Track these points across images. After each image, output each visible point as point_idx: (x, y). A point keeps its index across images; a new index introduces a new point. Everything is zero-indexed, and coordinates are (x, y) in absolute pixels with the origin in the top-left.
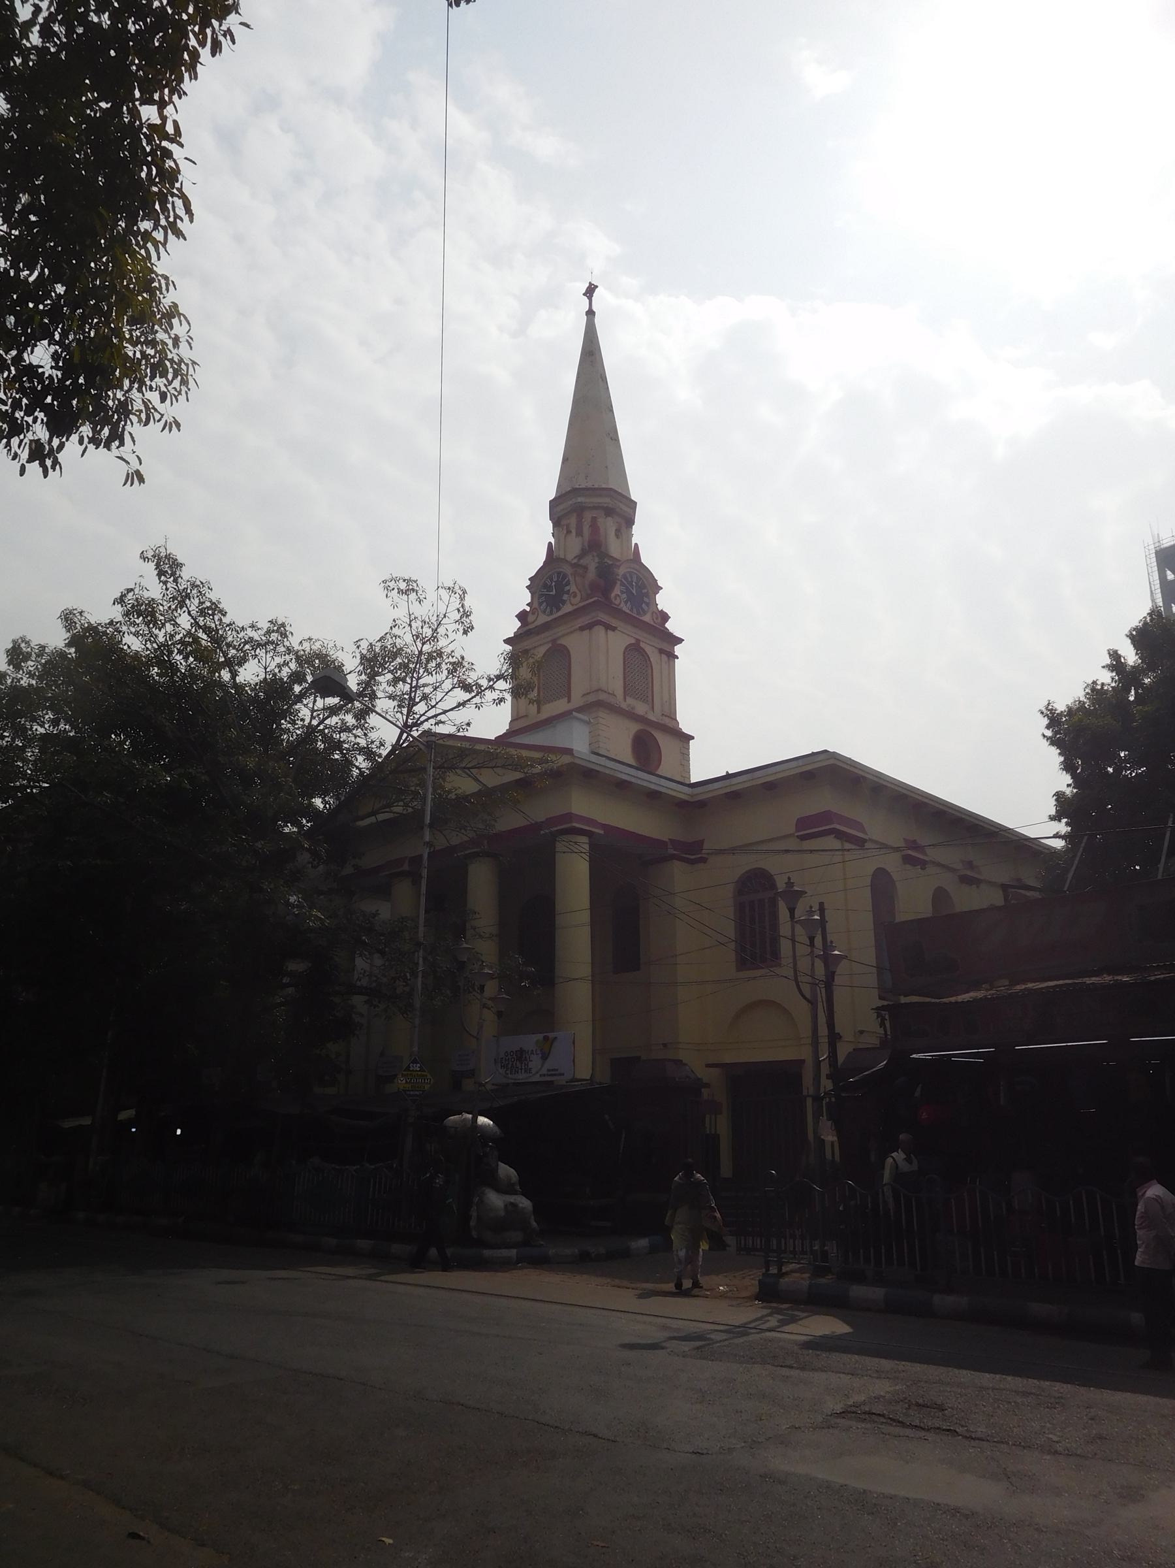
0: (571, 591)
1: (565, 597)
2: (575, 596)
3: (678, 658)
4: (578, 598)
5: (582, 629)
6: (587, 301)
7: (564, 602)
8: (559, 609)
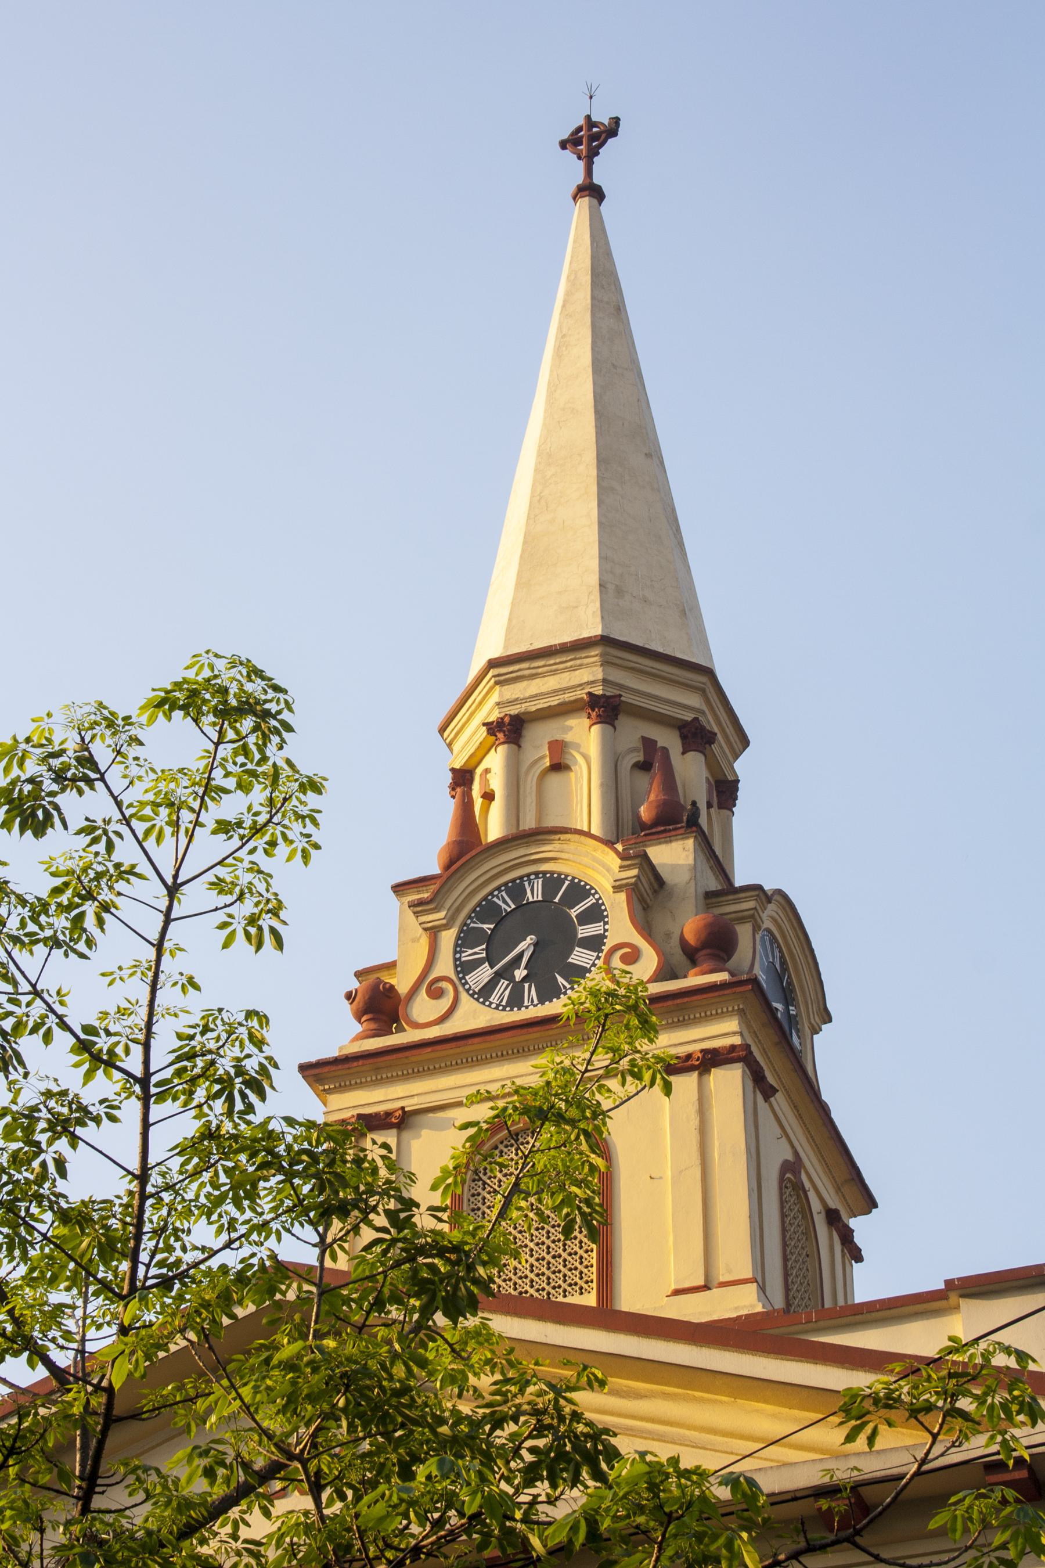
0: (609, 944)
1: (580, 957)
3: (859, 1259)
4: (649, 962)
6: (581, 165)
8: (549, 992)
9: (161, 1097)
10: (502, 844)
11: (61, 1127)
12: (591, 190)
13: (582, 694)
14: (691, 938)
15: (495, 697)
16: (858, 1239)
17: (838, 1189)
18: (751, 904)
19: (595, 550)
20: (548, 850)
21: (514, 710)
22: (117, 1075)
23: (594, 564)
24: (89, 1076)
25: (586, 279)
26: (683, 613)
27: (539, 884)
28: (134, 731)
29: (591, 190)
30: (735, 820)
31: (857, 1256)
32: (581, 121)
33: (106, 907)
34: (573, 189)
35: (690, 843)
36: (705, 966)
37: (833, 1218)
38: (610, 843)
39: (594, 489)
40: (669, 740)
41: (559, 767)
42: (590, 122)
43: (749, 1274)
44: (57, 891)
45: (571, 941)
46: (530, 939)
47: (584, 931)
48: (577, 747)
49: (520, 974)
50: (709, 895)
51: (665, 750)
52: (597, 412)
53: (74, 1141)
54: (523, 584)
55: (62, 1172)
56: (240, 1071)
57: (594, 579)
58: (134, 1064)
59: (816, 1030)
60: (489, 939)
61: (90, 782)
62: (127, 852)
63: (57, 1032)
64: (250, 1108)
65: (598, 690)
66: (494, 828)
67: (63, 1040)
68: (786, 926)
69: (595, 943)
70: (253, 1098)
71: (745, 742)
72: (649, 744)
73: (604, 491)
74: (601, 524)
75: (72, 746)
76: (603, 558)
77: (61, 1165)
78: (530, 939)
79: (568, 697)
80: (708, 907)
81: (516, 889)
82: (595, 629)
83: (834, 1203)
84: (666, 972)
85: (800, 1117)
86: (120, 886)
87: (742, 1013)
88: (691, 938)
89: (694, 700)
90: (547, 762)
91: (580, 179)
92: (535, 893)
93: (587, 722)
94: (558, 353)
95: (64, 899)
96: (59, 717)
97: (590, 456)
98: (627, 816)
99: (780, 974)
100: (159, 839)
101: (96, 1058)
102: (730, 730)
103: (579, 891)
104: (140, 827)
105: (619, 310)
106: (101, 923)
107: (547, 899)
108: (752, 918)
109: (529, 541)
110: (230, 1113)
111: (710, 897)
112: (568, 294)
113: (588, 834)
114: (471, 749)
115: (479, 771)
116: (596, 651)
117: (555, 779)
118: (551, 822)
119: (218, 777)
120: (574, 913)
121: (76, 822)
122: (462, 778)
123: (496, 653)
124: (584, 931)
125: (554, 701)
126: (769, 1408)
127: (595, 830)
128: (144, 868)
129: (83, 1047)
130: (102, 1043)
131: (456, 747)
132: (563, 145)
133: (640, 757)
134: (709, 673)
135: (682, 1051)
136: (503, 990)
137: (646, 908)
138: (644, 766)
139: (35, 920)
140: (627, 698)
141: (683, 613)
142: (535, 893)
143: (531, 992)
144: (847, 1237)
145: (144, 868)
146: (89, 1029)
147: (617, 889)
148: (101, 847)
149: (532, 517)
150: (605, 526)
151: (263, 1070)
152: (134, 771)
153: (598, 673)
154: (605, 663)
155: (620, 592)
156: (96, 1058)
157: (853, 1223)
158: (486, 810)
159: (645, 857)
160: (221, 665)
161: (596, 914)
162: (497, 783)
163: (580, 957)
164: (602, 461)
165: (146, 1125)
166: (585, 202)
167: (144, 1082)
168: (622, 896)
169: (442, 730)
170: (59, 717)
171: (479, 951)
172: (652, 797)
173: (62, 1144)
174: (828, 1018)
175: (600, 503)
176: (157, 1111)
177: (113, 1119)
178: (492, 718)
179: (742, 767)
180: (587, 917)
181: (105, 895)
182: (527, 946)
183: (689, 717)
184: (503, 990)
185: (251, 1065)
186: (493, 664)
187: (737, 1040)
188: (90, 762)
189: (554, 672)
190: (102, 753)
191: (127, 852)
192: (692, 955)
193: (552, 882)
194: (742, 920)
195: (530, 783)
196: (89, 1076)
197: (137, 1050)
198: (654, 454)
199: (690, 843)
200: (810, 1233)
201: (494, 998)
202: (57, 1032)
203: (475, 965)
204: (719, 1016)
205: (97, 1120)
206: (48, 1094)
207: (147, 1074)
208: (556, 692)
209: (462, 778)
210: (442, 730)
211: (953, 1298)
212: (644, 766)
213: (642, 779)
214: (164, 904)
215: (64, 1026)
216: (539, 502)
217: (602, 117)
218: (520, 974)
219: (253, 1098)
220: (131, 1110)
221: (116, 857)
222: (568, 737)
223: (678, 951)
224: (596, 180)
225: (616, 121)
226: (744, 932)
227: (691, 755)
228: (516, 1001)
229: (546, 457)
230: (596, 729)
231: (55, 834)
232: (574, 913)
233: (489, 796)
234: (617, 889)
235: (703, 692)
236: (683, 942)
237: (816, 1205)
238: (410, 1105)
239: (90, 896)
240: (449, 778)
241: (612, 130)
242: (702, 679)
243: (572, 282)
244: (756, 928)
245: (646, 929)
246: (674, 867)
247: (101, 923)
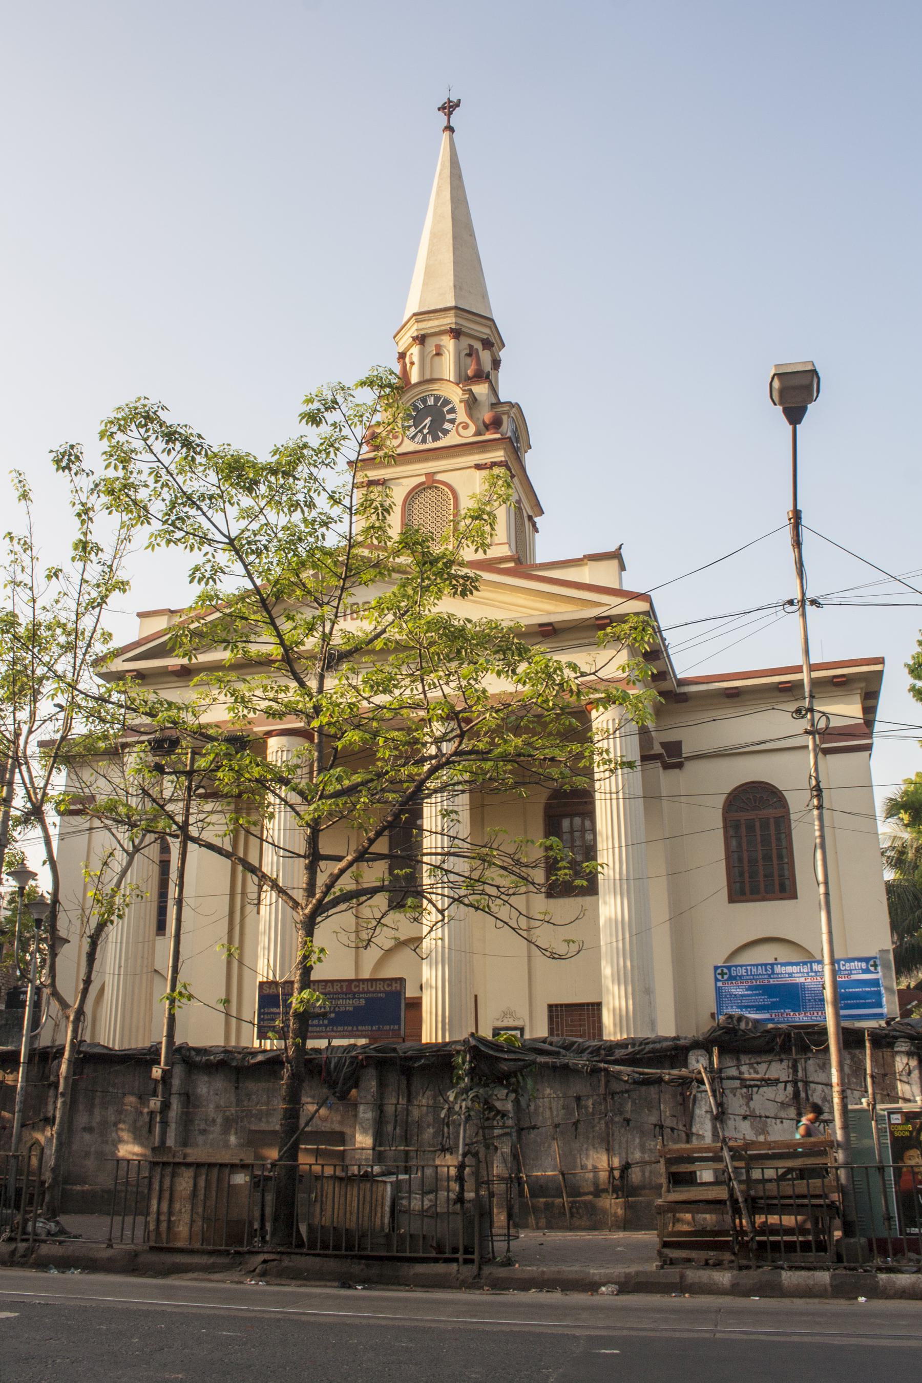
1: (447, 426)
2: (466, 427)
4: (472, 429)
5: (478, 467)
6: (446, 118)
7: (446, 432)
8: (436, 438)
9: (355, 514)
10: (419, 384)
11: (325, 524)
12: (450, 129)
13: (447, 327)
14: (487, 421)
15: (415, 327)
16: (538, 526)
17: (532, 508)
18: (507, 408)
19: (452, 272)
20: (435, 386)
21: (423, 332)
22: (341, 506)
23: (452, 278)
24: (332, 506)
25: (448, 164)
26: (483, 297)
27: (432, 398)
28: (351, 392)
29: (450, 129)
30: (500, 374)
31: (537, 531)
32: (446, 100)
33: (338, 449)
34: (443, 127)
35: (486, 385)
36: (492, 431)
37: (530, 518)
38: (457, 384)
39: (451, 248)
40: (478, 345)
41: (438, 354)
42: (450, 101)
43: (505, 541)
44: (322, 444)
45: (444, 420)
46: (429, 419)
47: (449, 417)
48: (445, 347)
49: (425, 431)
50: (492, 404)
51: (477, 350)
52: (453, 218)
53: (328, 528)
54: (425, 284)
55: (324, 539)
56: (382, 506)
57: (451, 284)
58: (346, 502)
59: (526, 452)
60: (414, 418)
61: (335, 409)
62: (346, 431)
63: (322, 492)
64: (385, 518)
65: (453, 326)
66: (414, 378)
67: (324, 495)
68: (518, 415)
69: (452, 421)
70: (386, 514)
71: (504, 346)
72: (471, 347)
73: (455, 249)
74: (454, 262)
75: (330, 397)
76: (455, 276)
77: (323, 536)
78: (429, 419)
79: (442, 328)
80: (492, 408)
81: (424, 400)
82: (452, 303)
83: (530, 514)
84: (478, 433)
85: (521, 484)
86: (342, 442)
87: (505, 449)
88: (487, 421)
89: (487, 331)
90: (434, 352)
91: (445, 124)
92: (431, 402)
93: (448, 338)
94: (438, 194)
95: (323, 447)
96: (325, 387)
97: (450, 235)
98: (463, 374)
99: (515, 432)
100: (355, 426)
101: (335, 501)
102: (499, 341)
103: (447, 402)
104: (350, 422)
105: (460, 177)
106: (336, 454)
107: (435, 404)
108: (507, 413)
109: (428, 267)
110: (378, 519)
111: (493, 405)
112: (441, 170)
113: (449, 381)
114: (406, 345)
115: (408, 354)
116: (453, 312)
117: (437, 358)
118: (436, 376)
119: (378, 407)
120: (445, 410)
121: (330, 422)
122: (402, 356)
123: (416, 310)
124: (449, 417)
125: (437, 330)
126: (523, 596)
127: (452, 379)
128: (351, 436)
129: (331, 497)
130: (337, 496)
131: (400, 344)
132: (439, 109)
133: (467, 351)
134: (492, 320)
135: (484, 462)
136: (419, 437)
137: (470, 408)
138: (469, 355)
139: (317, 455)
140: (464, 329)
141: (483, 297)
142: (431, 402)
143: (429, 438)
144: (534, 525)
145: (351, 436)
146: (334, 492)
147: (461, 402)
148: (338, 430)
149: (428, 258)
150: (456, 263)
151: (390, 506)
152: (350, 405)
153: (453, 320)
154: (456, 316)
155: (461, 289)
156: (335, 501)
157: (536, 519)
158: (411, 368)
159: (471, 390)
160: (380, 369)
161: (453, 410)
162: (416, 359)
163: (447, 426)
164: (455, 237)
165: (351, 523)
166: (447, 133)
167: (350, 509)
168: (463, 405)
169: (394, 337)
170: (325, 387)
171: (411, 422)
172: (473, 367)
173: (324, 529)
174: (530, 447)
175: (454, 254)
176: (354, 518)
177: (341, 521)
178: (415, 334)
179: (502, 354)
180: (450, 412)
181: (337, 445)
182: (428, 421)
183: (485, 337)
184: (419, 437)
185: (387, 504)
186: (415, 315)
187: (503, 459)
188: (335, 402)
189: (437, 319)
190: (340, 400)
191: (346, 431)
192: (487, 427)
193: (437, 398)
194: (504, 414)
195: (428, 359)
196: (332, 506)
197: (348, 498)
198: (472, 235)
199: (486, 385)
200: (523, 524)
201: (416, 440)
202: (322, 492)
203: (410, 427)
204: (497, 450)
205: (336, 522)
206: (320, 513)
207: (352, 506)
208: (438, 326)
209: (402, 356)
210: (394, 337)
211: (586, 561)
212: (469, 355)
213: (469, 360)
214: (357, 449)
215: (324, 490)
216: (431, 253)
217: (454, 99)
218: (425, 431)
219: (386, 514)
220: (346, 517)
221: (343, 434)
222: (442, 343)
223: (482, 425)
224: (452, 125)
225: (459, 101)
226: (505, 418)
227: (486, 351)
228: (424, 441)
229: (433, 235)
230: (452, 341)
231: (323, 426)
232: (445, 410)
233: (412, 363)
234: (461, 402)
235: (490, 327)
236: (484, 422)
237: (525, 515)
238: (387, 477)
239: (332, 445)
240: (397, 355)
241: (458, 104)
242: (489, 323)
243: (443, 165)
244: (509, 417)
245: (470, 415)
246: (481, 394)
247: (336, 454)
